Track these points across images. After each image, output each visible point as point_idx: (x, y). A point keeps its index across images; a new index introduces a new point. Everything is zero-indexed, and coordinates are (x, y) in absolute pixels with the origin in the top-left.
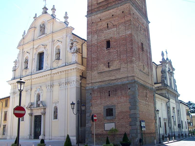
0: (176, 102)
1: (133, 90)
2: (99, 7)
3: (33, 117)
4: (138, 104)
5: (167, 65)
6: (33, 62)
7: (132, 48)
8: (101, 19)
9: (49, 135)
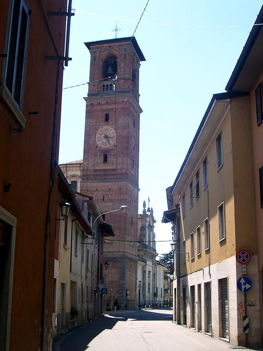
0: (152, 264)
1: (123, 264)
2: (96, 175)
4: (126, 276)
5: (148, 219)
7: (125, 226)
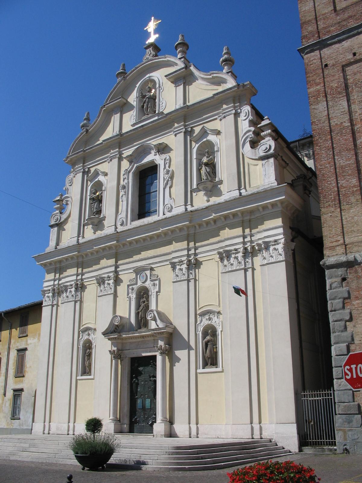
3: (127, 362)
6: (122, 193)
8: (354, 54)
9: (190, 434)
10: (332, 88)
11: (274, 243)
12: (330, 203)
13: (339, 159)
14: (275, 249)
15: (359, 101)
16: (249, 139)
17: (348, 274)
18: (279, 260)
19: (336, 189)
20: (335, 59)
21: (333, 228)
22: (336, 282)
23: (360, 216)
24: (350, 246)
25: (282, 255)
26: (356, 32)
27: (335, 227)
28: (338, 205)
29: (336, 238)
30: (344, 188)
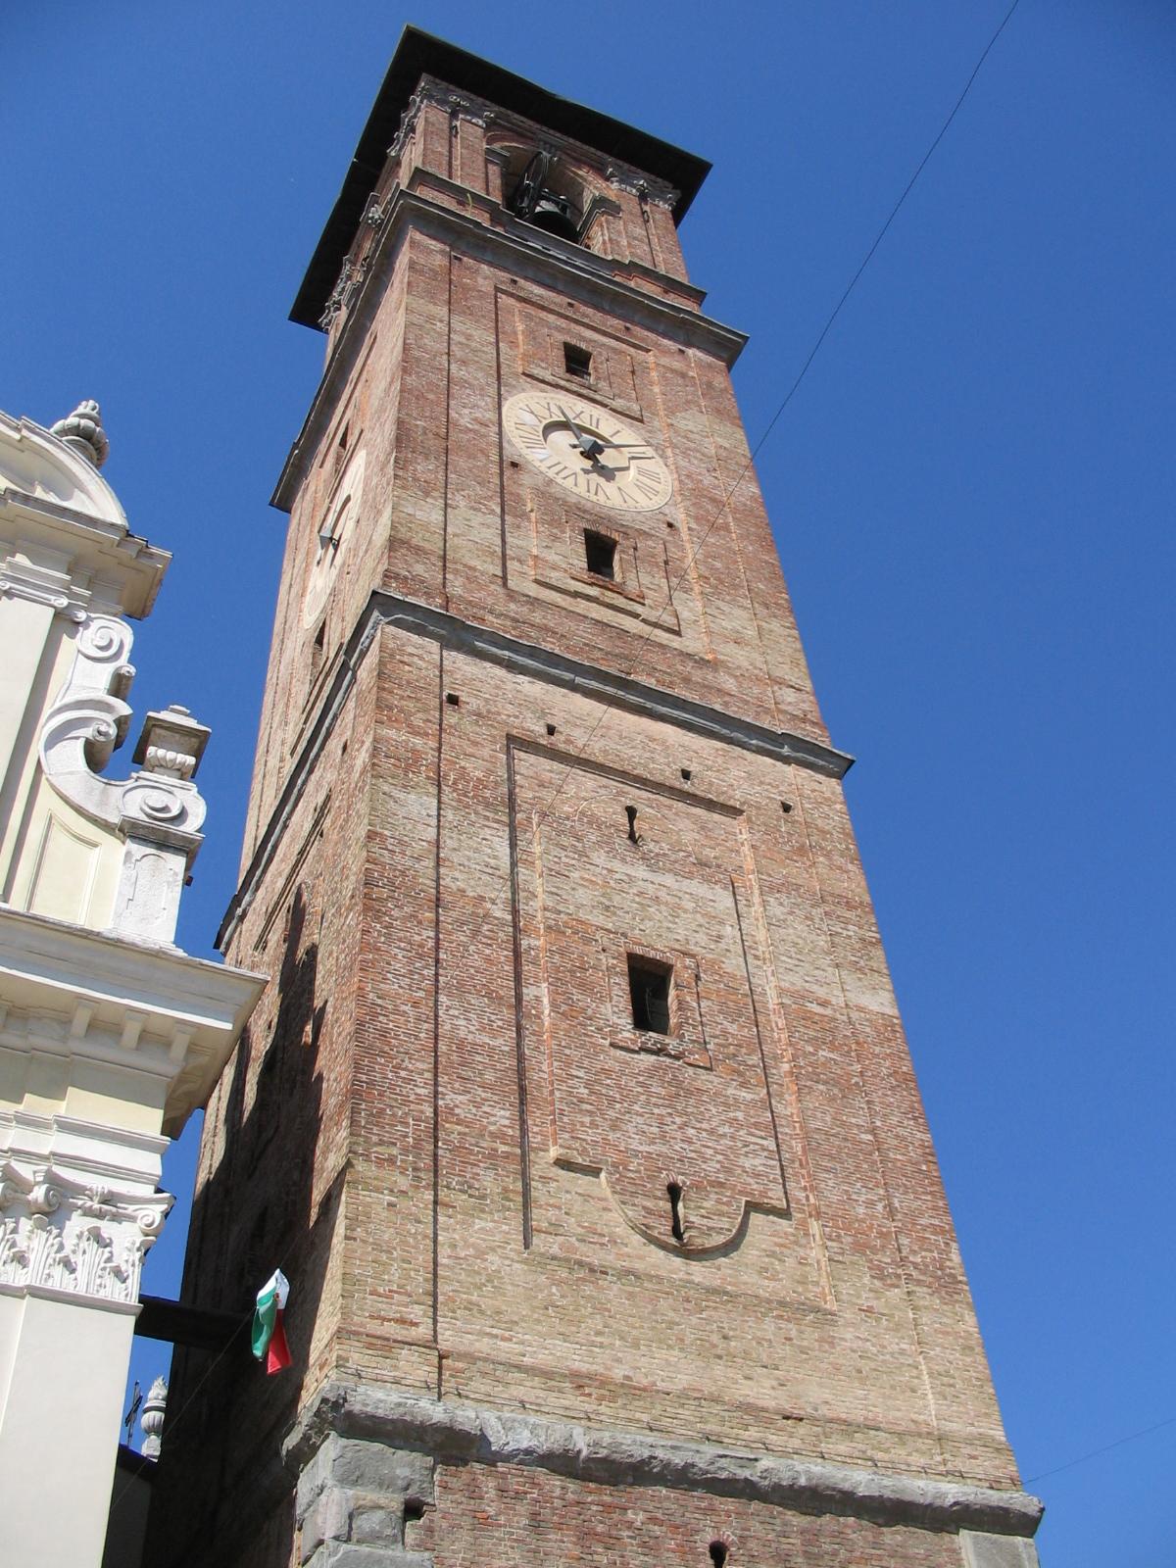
10: (463, 774)
11: (97, 1206)
12: (395, 1151)
13: (456, 1013)
14: (96, 1237)
15: (551, 870)
16: (88, 732)
17: (436, 1488)
18: (102, 1295)
19: (429, 1111)
20: (487, 700)
21: (393, 1259)
22: (383, 1508)
23: (512, 1260)
24: (460, 1365)
25: (129, 1281)
26: (568, 676)
27: (403, 1261)
28: (427, 1177)
29: (403, 1305)
30: (457, 1124)
